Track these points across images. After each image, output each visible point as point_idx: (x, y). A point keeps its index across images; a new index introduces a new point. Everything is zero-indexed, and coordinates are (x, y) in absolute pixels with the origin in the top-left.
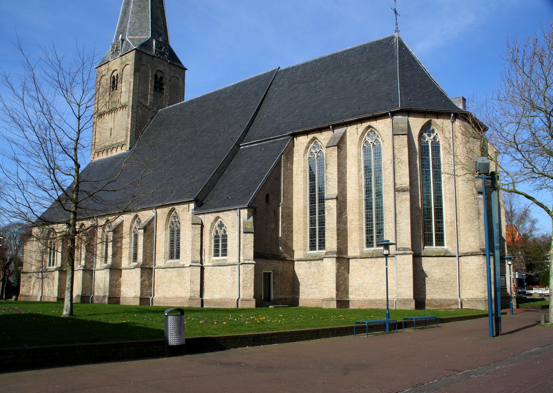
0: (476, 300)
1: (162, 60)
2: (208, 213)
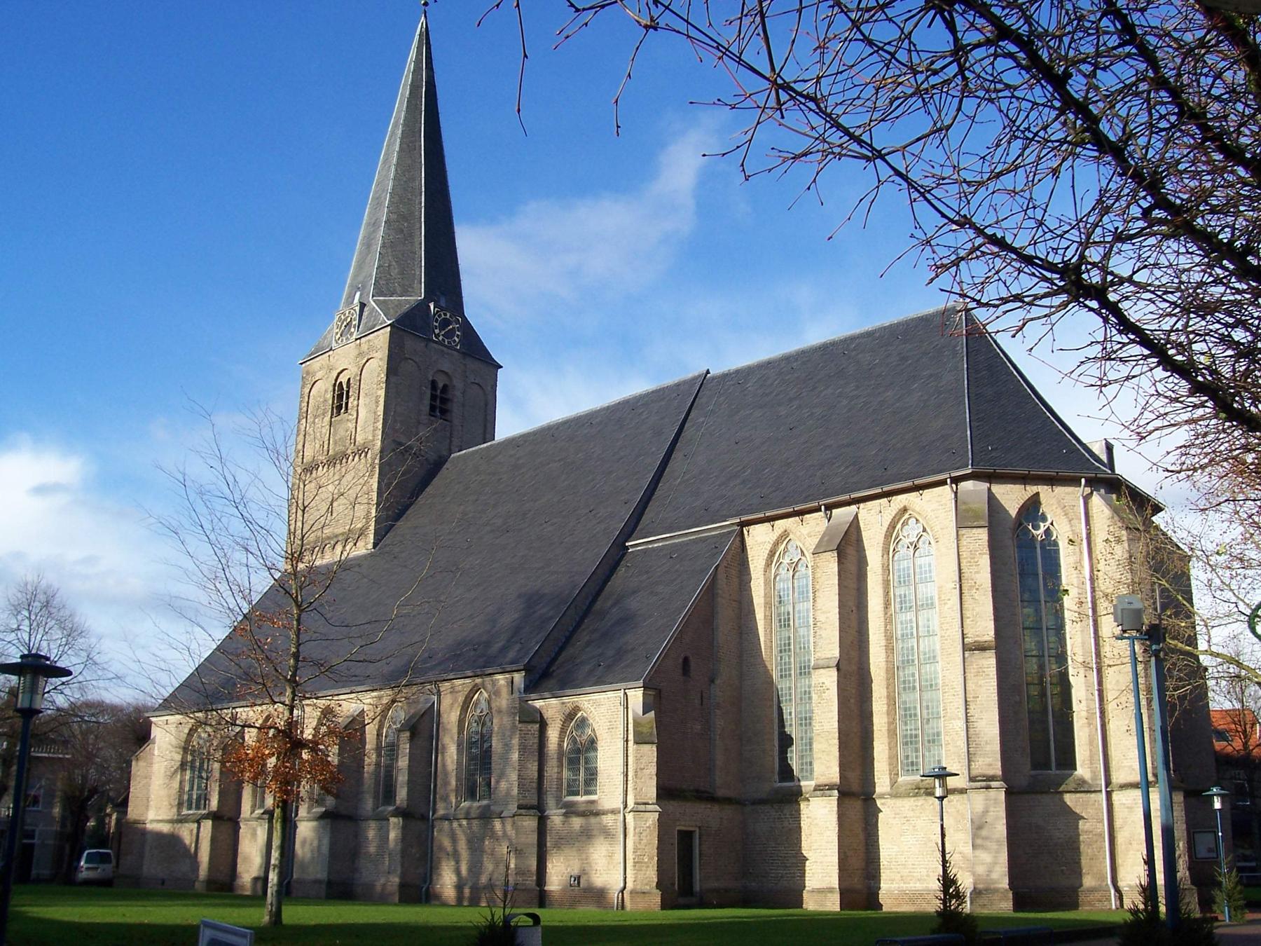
1: (446, 346)
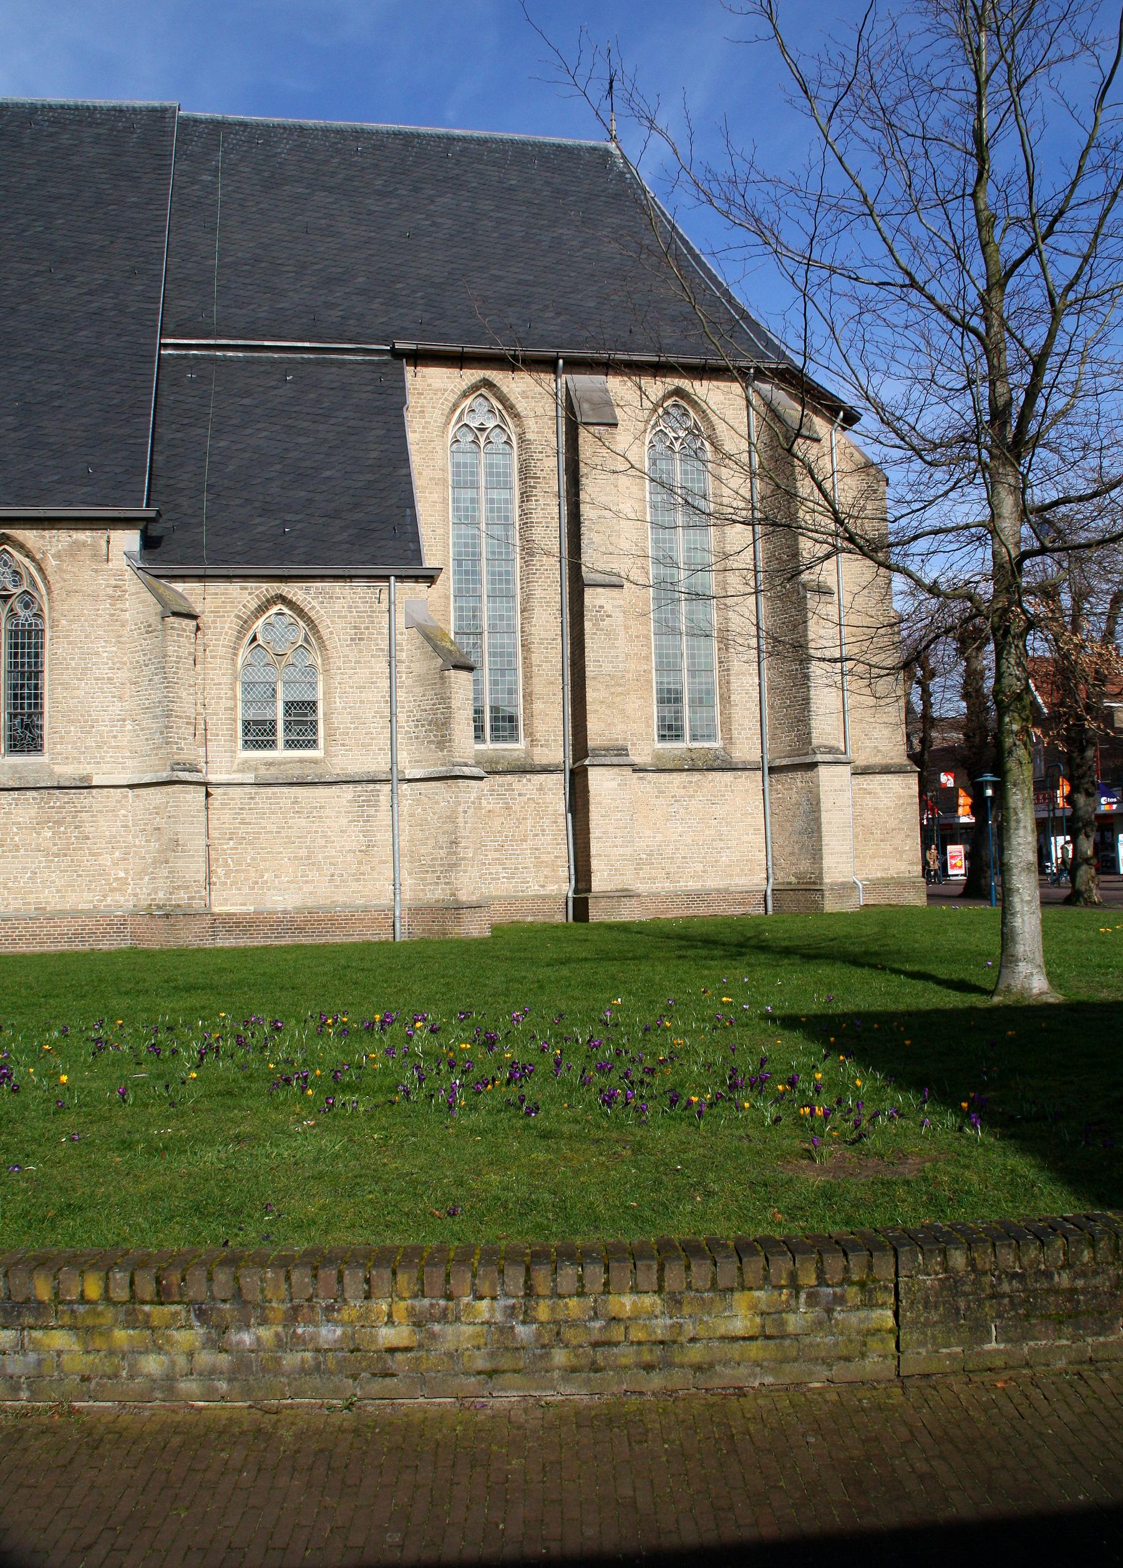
0: (899, 883)
2: (228, 578)
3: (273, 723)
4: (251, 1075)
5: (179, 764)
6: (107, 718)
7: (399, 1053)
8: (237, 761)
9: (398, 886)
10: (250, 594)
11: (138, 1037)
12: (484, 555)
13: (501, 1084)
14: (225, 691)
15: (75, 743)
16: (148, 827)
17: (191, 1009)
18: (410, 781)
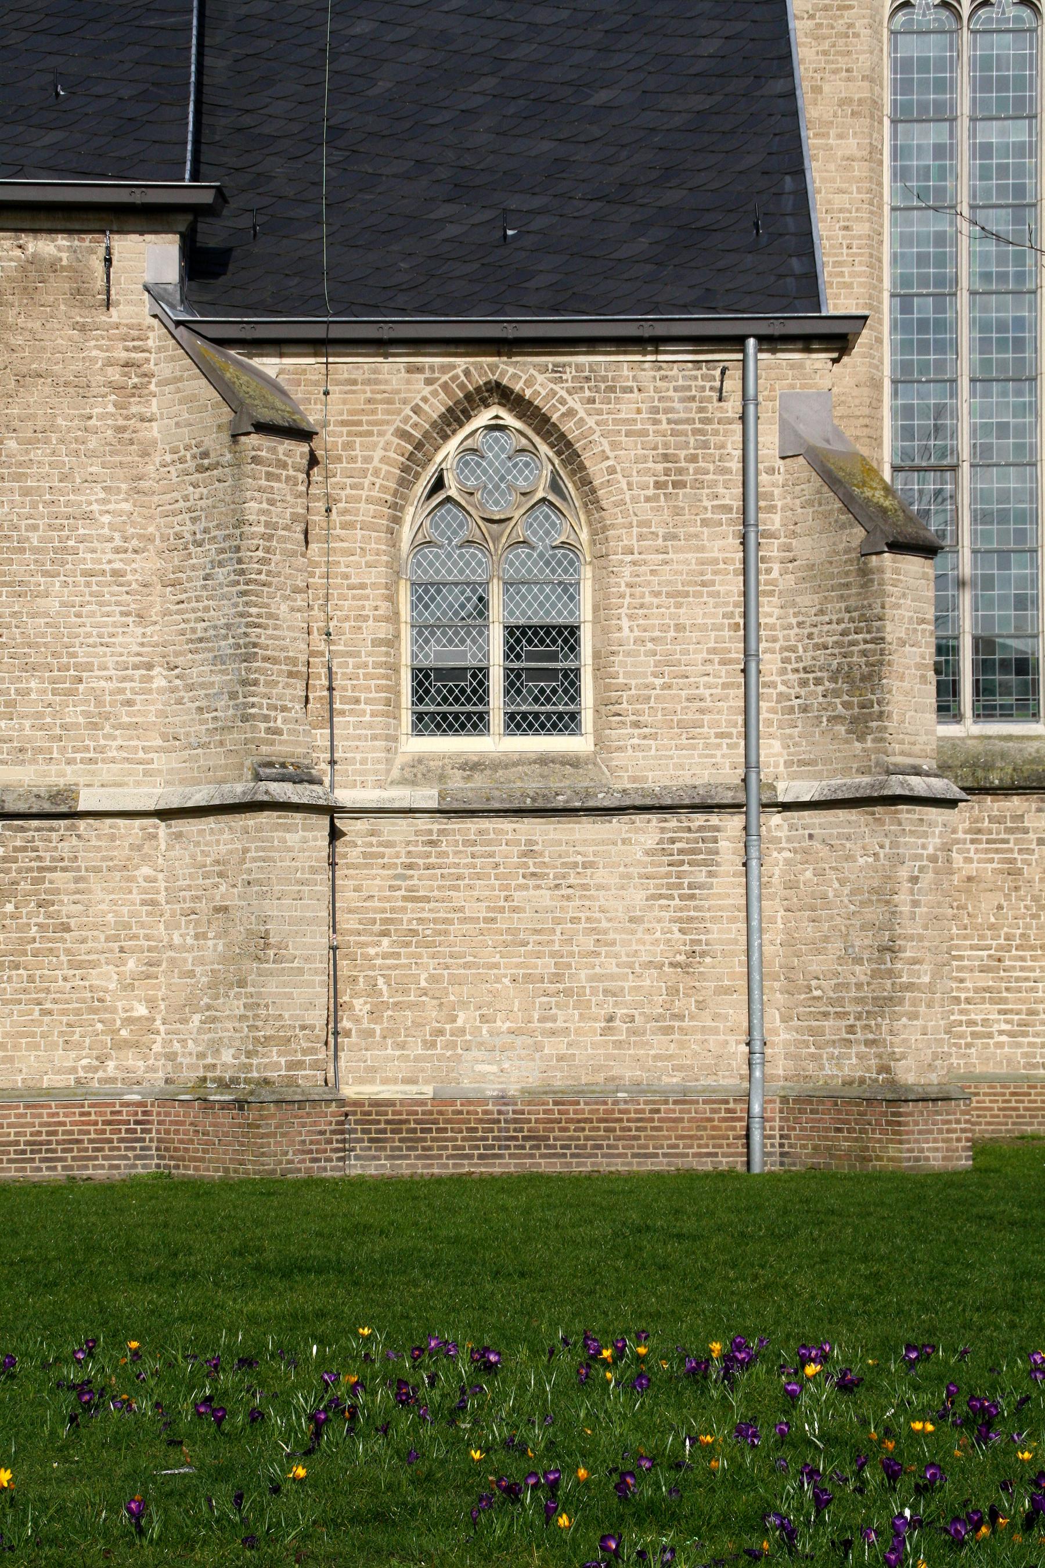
2: (381, 345)
3: (480, 674)
4: (429, 1476)
5: (270, 765)
6: (110, 662)
7: (767, 1435)
8: (399, 761)
9: (757, 1046)
10: (429, 382)
11: (174, 1379)
12: (964, 283)
13: (1012, 1525)
14: (374, 602)
15: (39, 715)
16: (202, 906)
17: (294, 1316)
18: (786, 807)
